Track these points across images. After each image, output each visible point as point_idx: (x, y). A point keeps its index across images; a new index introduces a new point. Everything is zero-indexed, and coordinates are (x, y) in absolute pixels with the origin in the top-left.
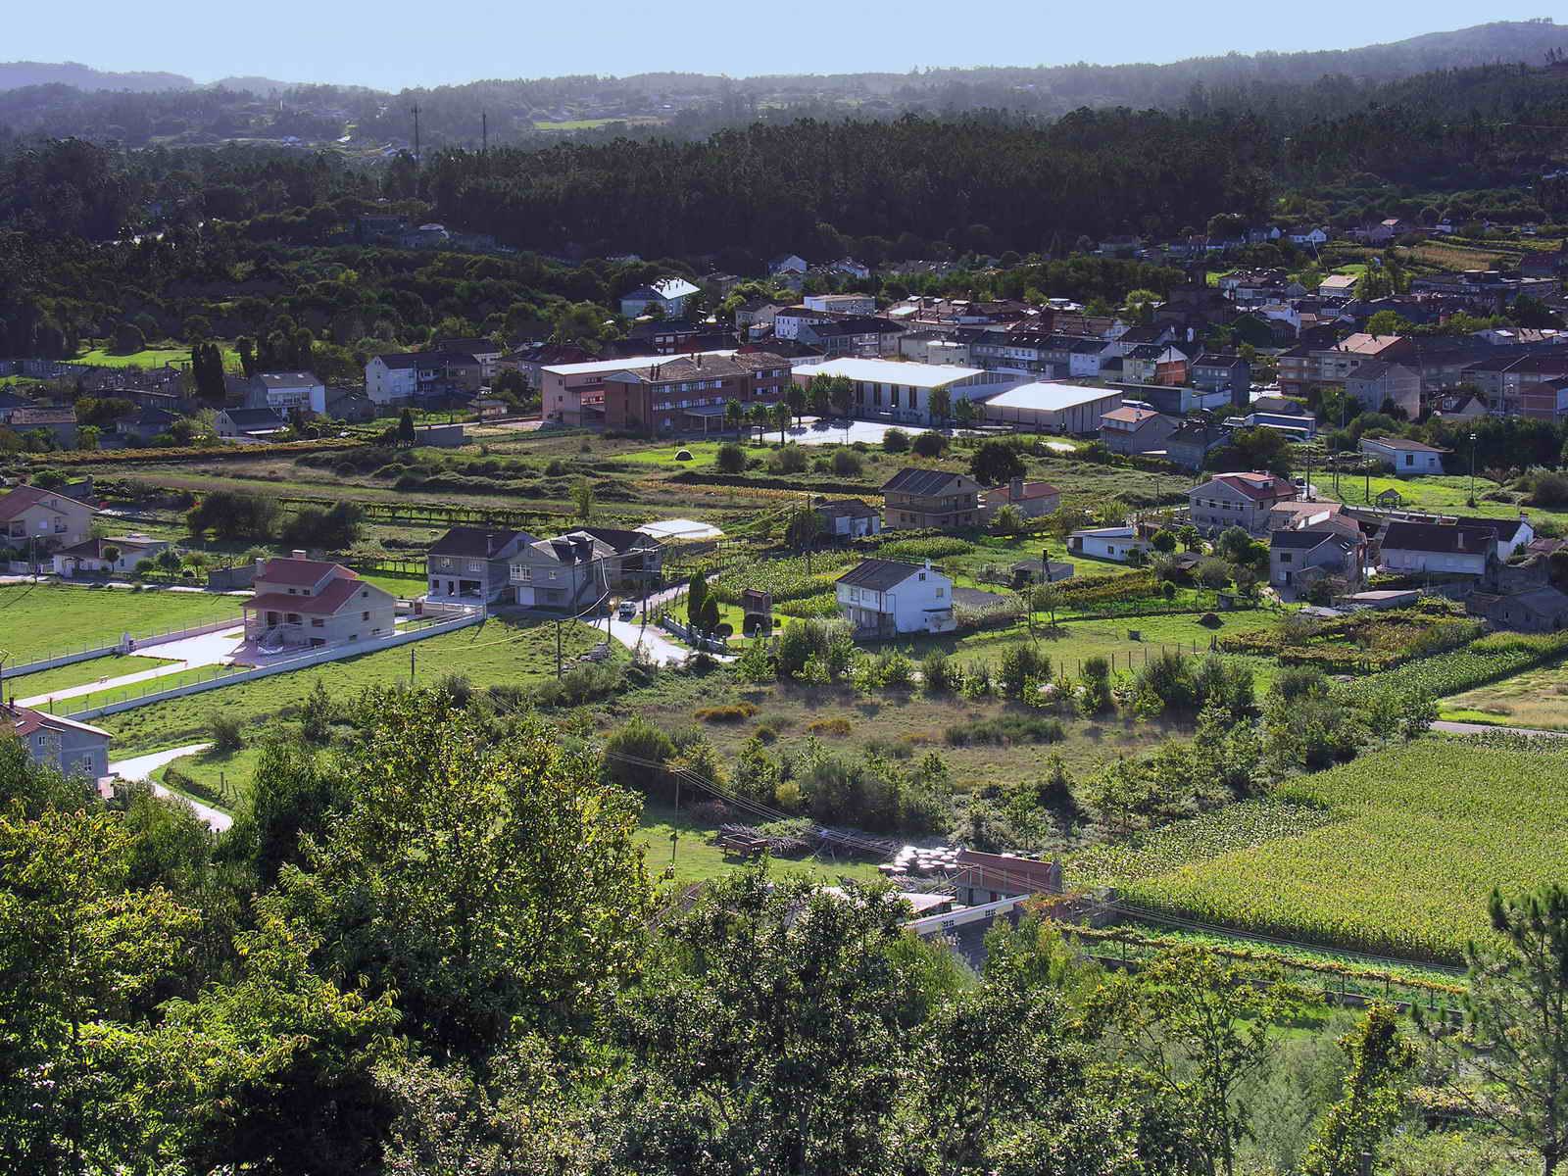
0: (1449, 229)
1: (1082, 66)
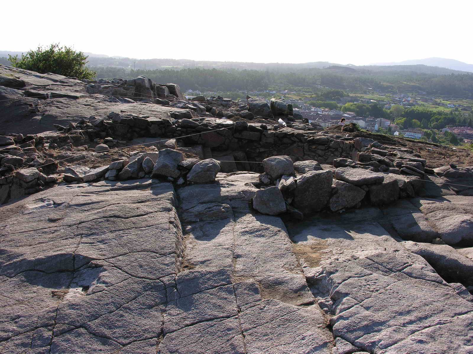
0: (295, 93)
1: (278, 63)
